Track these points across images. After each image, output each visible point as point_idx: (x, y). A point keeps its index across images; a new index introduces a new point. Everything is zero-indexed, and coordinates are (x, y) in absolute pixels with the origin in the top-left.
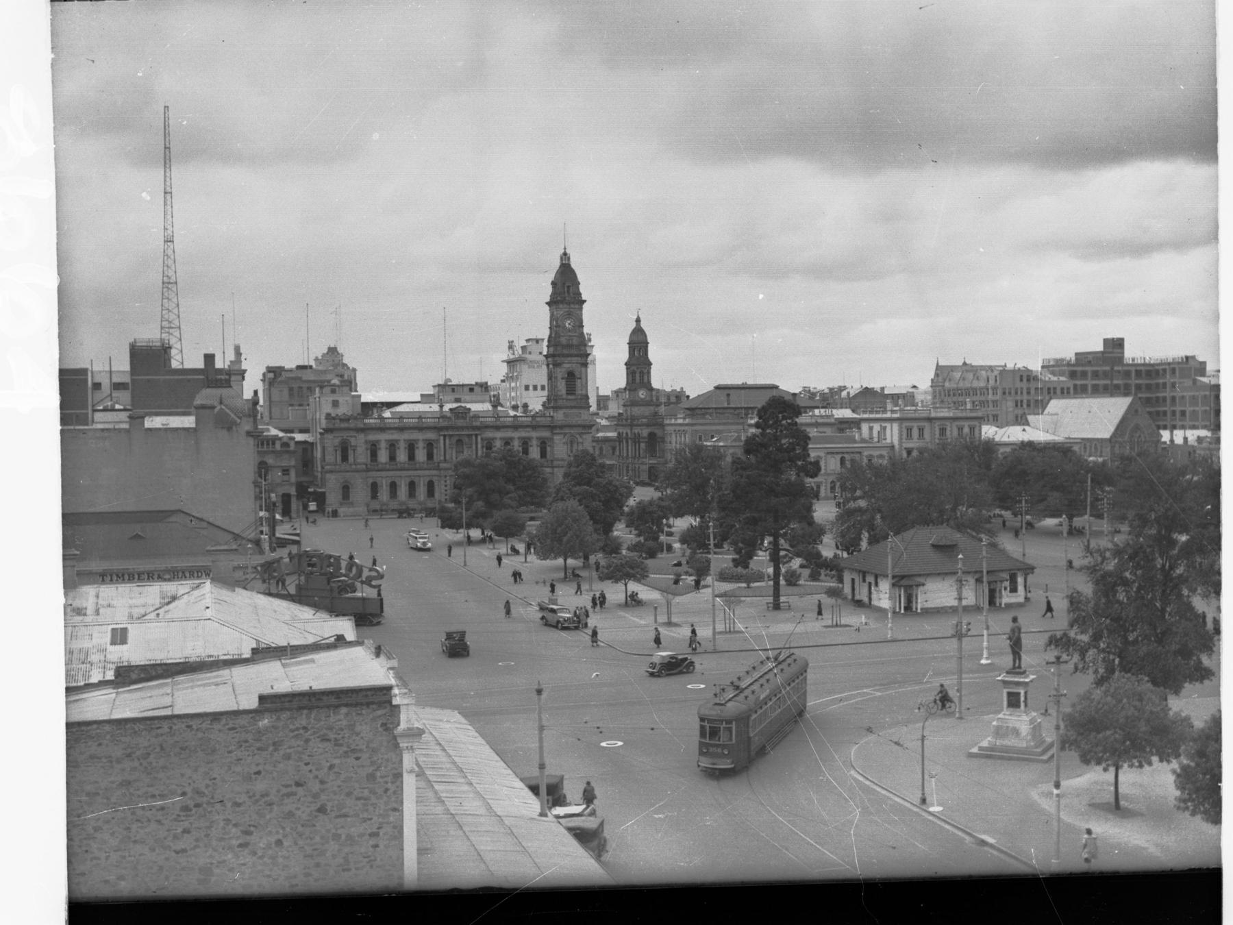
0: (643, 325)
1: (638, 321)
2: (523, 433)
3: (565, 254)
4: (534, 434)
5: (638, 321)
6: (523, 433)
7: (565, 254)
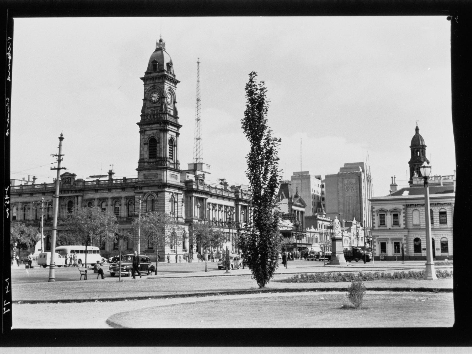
0: (420, 132)
1: (417, 129)
2: (115, 194)
3: (161, 41)
4: (123, 194)
5: (417, 129)
6: (115, 194)
7: (161, 41)
